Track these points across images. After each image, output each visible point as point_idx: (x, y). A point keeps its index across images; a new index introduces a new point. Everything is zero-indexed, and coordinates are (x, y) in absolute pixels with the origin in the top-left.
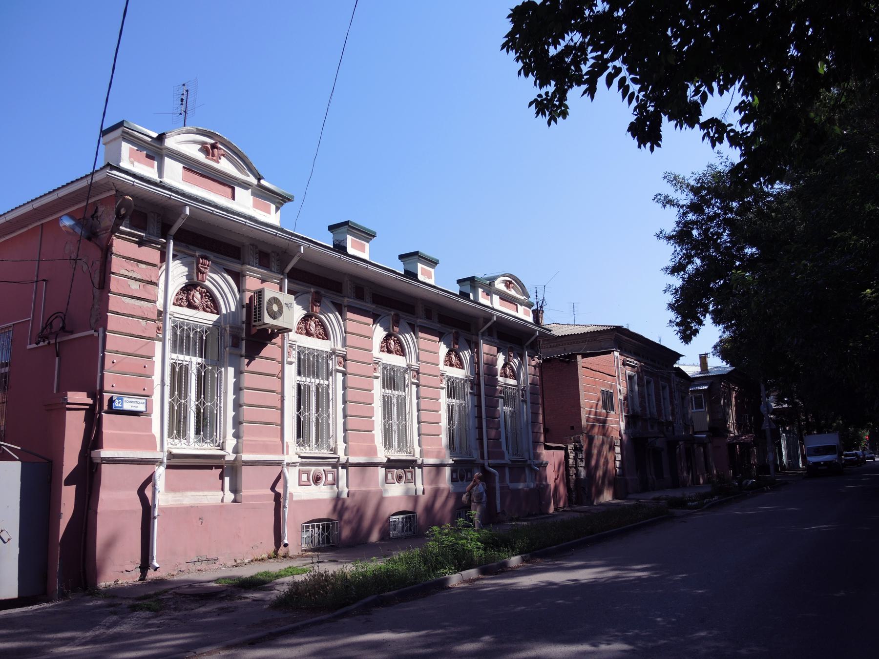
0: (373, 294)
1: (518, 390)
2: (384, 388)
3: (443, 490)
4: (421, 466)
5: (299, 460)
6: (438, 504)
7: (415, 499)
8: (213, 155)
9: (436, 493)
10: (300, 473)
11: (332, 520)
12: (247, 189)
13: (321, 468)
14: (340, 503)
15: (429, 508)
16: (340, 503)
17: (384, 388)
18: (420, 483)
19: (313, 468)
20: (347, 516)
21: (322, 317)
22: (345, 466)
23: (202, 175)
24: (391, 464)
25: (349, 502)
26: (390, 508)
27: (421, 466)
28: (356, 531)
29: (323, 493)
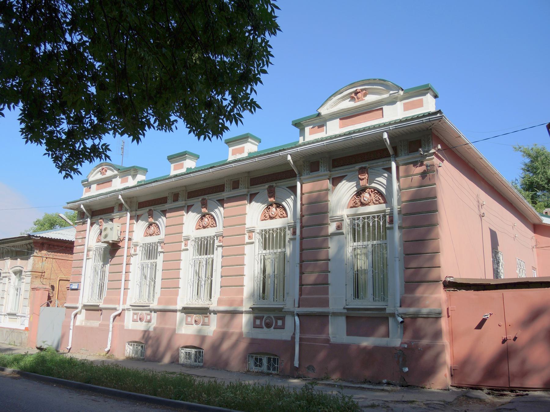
0: (239, 181)
1: (384, 216)
2: (265, 249)
3: (232, 334)
4: (215, 312)
5: (131, 307)
6: (226, 346)
7: (203, 338)
8: (358, 99)
9: (224, 336)
10: (134, 314)
11: (141, 343)
12: (116, 177)
13: (144, 312)
14: (147, 333)
15: (216, 347)
16: (147, 333)
17: (265, 249)
18: (212, 327)
19: (140, 312)
20: (150, 342)
21: (373, 185)
22: (155, 311)
23: (103, 183)
24: (187, 311)
25: (152, 334)
26: (179, 342)
27: (215, 312)
28: (155, 353)
29: (141, 326)
